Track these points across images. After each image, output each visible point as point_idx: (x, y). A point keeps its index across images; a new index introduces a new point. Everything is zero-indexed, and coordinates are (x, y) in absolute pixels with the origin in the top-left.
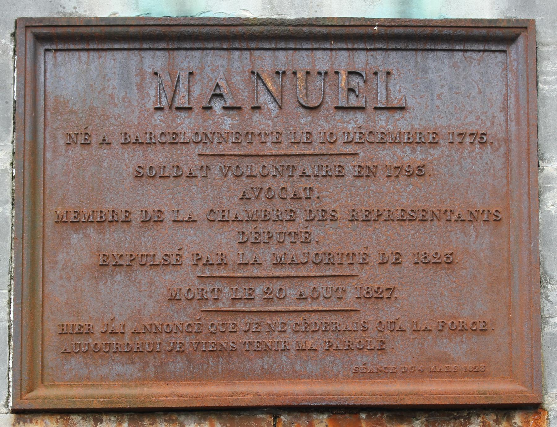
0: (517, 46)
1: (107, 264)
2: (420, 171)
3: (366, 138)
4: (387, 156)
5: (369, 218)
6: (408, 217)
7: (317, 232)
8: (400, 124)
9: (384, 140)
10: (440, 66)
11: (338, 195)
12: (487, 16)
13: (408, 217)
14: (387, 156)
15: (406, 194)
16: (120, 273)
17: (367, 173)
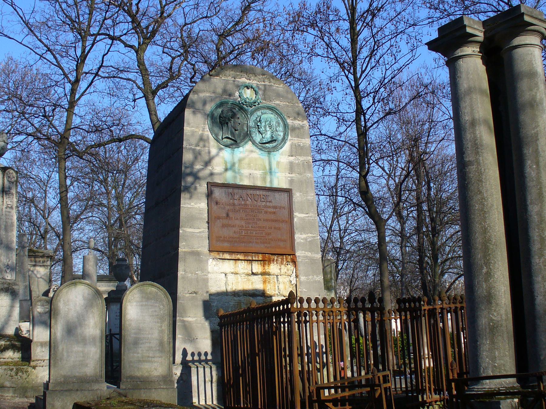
0: (45, 281)
1: (224, 226)
2: (274, 213)
3: (266, 206)
4: (269, 210)
5: (267, 220)
6: (273, 221)
7: (258, 223)
8: (271, 204)
9: (270, 207)
10: (277, 195)
11: (262, 216)
12: (285, 187)
13: (273, 221)
14: (269, 210)
15: (272, 217)
16: (277, 260)
17: (266, 212)
